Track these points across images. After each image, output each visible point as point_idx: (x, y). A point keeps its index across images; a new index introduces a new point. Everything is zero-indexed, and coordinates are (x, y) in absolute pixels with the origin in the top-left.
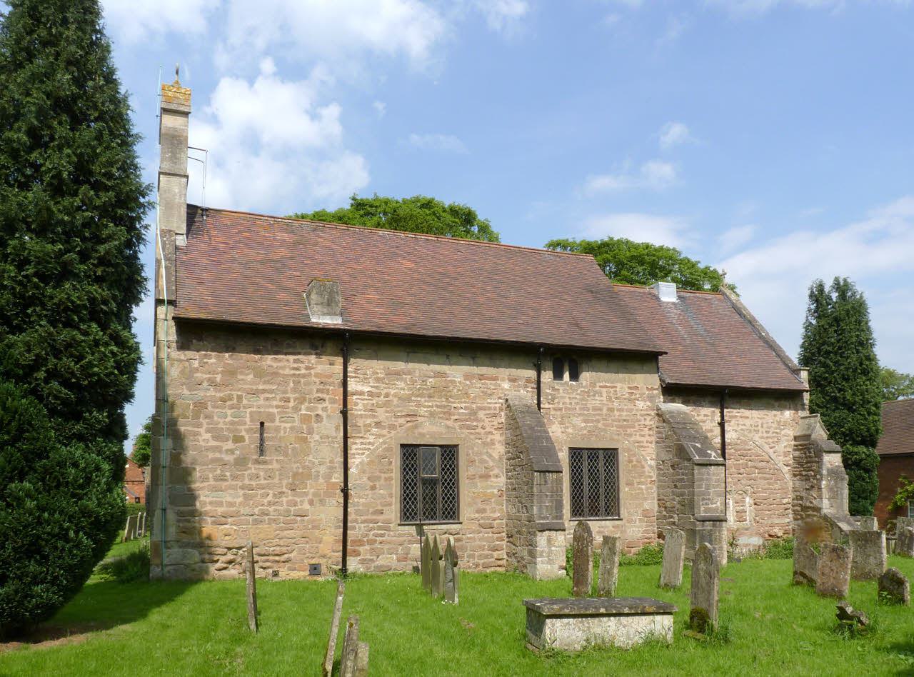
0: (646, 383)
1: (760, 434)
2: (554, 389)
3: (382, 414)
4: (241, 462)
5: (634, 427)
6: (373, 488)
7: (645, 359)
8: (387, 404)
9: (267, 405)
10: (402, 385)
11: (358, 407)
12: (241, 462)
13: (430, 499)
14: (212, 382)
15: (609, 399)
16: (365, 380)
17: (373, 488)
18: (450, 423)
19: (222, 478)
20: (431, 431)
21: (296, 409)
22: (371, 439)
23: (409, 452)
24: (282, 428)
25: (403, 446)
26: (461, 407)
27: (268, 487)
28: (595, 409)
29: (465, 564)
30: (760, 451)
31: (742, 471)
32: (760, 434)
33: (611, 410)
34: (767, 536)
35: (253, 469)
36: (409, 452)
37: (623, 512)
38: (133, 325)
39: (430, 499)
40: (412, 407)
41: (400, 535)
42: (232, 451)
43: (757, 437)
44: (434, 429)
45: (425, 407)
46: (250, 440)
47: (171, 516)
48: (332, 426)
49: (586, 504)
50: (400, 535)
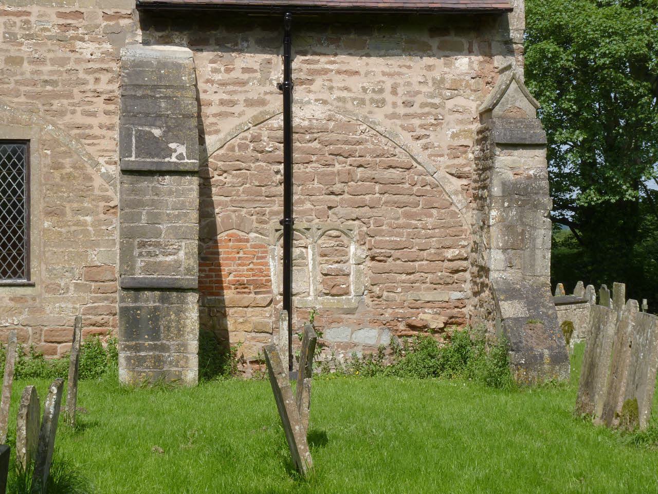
1: (388, 109)
5: (70, 96)
30: (389, 147)
31: (338, 187)
32: (388, 109)
34: (402, 326)
37: (38, 269)
43: (379, 116)
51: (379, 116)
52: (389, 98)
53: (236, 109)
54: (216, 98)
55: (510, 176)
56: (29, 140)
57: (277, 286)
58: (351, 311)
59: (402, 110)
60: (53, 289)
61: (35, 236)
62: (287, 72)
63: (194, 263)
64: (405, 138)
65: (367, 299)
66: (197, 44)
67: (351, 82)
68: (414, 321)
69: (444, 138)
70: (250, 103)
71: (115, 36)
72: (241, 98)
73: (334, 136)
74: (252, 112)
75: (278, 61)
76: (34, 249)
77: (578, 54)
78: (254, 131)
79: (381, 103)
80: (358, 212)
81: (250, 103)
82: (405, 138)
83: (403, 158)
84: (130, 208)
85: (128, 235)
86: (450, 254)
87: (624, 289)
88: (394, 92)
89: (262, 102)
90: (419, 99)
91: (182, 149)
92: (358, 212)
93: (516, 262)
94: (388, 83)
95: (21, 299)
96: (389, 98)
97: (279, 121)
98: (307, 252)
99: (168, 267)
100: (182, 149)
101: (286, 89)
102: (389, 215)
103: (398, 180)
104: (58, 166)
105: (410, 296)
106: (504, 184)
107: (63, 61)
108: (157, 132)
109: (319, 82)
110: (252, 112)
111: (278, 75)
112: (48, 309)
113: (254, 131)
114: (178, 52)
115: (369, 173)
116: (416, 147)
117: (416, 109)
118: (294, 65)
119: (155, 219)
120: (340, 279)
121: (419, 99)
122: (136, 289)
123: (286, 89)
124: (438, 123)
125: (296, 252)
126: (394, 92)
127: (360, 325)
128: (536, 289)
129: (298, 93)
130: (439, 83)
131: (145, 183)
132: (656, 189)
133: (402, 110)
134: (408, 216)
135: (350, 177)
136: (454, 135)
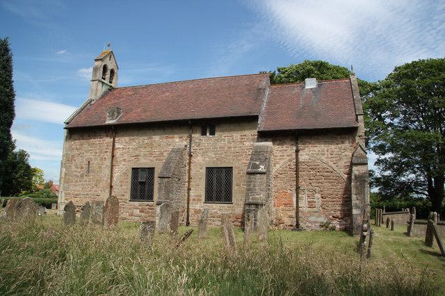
0: (251, 133)
1: (326, 156)
2: (200, 139)
3: (126, 157)
4: (82, 176)
5: (242, 156)
6: (121, 186)
7: (250, 120)
8: (128, 152)
9: (89, 155)
10: (134, 144)
11: (118, 153)
12: (82, 176)
13: (142, 191)
14: (77, 149)
15: (229, 142)
16: (121, 144)
17: (121, 186)
18: (151, 158)
19: (77, 182)
20: (144, 162)
21: (99, 156)
22: (122, 166)
23: (135, 170)
24: (95, 163)
25: (133, 169)
26: (157, 151)
27: (89, 185)
28: (221, 148)
29: (56, 183)
30: (327, 166)
31: (312, 178)
32: (326, 156)
33: (230, 148)
34: (331, 217)
35: (85, 178)
36: (135, 170)
37: (234, 200)
38: (247, 133)
39: (142, 191)
40: (137, 153)
41: (130, 205)
42: (79, 172)
43: (323, 158)
44: (145, 161)
45: (143, 151)
46: (85, 167)
47: (63, 194)
48: (108, 162)
49: (214, 195)
50: (130, 205)
52: (326, 153)
53: (285, 157)
54: (279, 155)
55: (357, 173)
56: (232, 168)
65: (321, 208)
66: (274, 141)
68: (335, 215)
73: (311, 164)
74: (288, 158)
76: (233, 195)
77: (399, 172)
78: (289, 163)
79: (323, 154)
80: (317, 185)
81: (288, 156)
82: (331, 164)
83: (331, 170)
89: (291, 155)
92: (317, 185)
96: (326, 153)
104: (239, 173)
106: (355, 176)
108: (257, 163)
110: (288, 158)
112: (236, 210)
113: (289, 163)
114: (269, 144)
116: (334, 166)
117: (334, 156)
119: (254, 186)
120: (313, 203)
121: (335, 153)
124: (340, 159)
125: (300, 196)
131: (252, 177)
132: (438, 55)
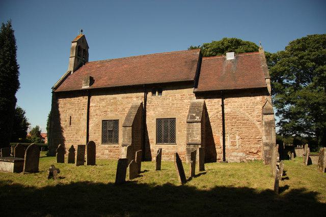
31: (233, 125)
37: (177, 141)
51: (241, 110)
52: (243, 106)
57: (222, 145)
58: (236, 149)
59: (246, 109)
60: (180, 145)
61: (177, 135)
62: (223, 102)
63: (200, 139)
64: (247, 114)
65: (240, 147)
67: (236, 104)
69: (255, 114)
70: (215, 109)
71: (190, 98)
72: (214, 108)
75: (220, 100)
76: (177, 138)
81: (215, 109)
84: (188, 129)
85: (188, 134)
86: (257, 137)
87: (180, 178)
88: (244, 105)
90: (250, 106)
91: (198, 118)
93: (268, 138)
94: (243, 104)
95: (174, 147)
97: (221, 112)
98: (228, 137)
99: (195, 140)
100: (198, 118)
101: (223, 106)
102: (244, 130)
103: (246, 122)
105: (249, 146)
107: (182, 103)
108: (194, 115)
109: (229, 104)
111: (221, 103)
115: (240, 121)
118: (224, 101)
119: (193, 131)
121: (250, 106)
122: (189, 144)
123: (223, 106)
124: (254, 111)
126: (244, 105)
127: (239, 152)
128: (272, 144)
129: (225, 106)
130: (254, 103)
131: (191, 124)
133: (246, 109)
134: (248, 130)
135: (236, 123)
136: (257, 113)
